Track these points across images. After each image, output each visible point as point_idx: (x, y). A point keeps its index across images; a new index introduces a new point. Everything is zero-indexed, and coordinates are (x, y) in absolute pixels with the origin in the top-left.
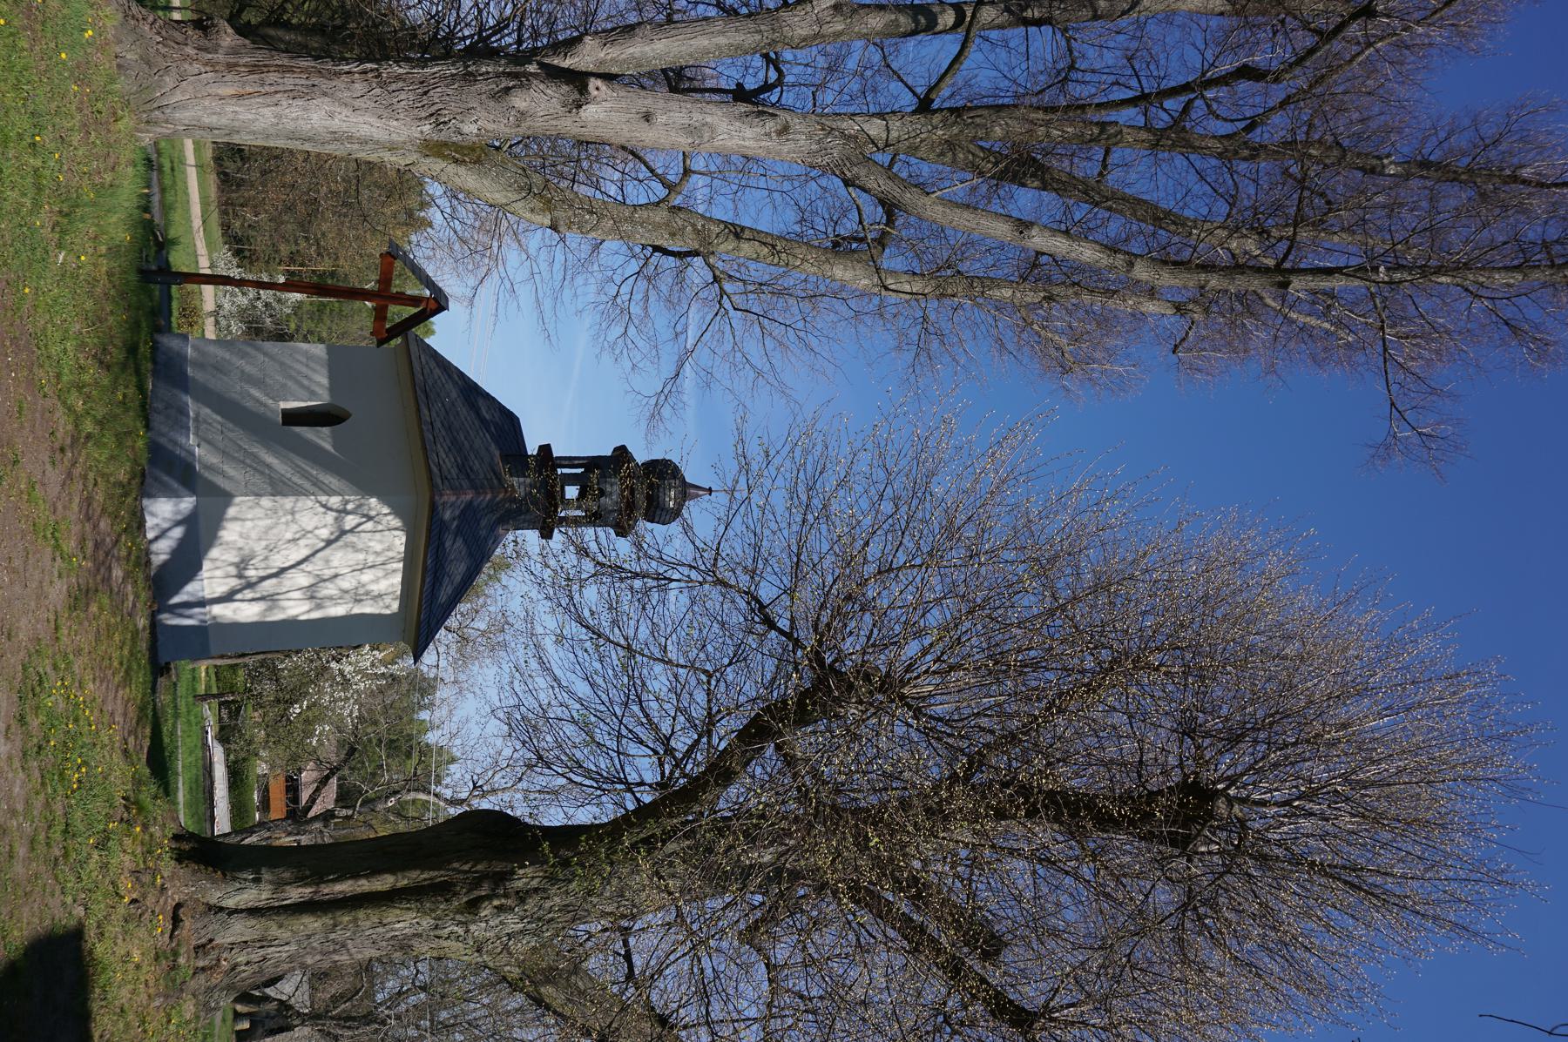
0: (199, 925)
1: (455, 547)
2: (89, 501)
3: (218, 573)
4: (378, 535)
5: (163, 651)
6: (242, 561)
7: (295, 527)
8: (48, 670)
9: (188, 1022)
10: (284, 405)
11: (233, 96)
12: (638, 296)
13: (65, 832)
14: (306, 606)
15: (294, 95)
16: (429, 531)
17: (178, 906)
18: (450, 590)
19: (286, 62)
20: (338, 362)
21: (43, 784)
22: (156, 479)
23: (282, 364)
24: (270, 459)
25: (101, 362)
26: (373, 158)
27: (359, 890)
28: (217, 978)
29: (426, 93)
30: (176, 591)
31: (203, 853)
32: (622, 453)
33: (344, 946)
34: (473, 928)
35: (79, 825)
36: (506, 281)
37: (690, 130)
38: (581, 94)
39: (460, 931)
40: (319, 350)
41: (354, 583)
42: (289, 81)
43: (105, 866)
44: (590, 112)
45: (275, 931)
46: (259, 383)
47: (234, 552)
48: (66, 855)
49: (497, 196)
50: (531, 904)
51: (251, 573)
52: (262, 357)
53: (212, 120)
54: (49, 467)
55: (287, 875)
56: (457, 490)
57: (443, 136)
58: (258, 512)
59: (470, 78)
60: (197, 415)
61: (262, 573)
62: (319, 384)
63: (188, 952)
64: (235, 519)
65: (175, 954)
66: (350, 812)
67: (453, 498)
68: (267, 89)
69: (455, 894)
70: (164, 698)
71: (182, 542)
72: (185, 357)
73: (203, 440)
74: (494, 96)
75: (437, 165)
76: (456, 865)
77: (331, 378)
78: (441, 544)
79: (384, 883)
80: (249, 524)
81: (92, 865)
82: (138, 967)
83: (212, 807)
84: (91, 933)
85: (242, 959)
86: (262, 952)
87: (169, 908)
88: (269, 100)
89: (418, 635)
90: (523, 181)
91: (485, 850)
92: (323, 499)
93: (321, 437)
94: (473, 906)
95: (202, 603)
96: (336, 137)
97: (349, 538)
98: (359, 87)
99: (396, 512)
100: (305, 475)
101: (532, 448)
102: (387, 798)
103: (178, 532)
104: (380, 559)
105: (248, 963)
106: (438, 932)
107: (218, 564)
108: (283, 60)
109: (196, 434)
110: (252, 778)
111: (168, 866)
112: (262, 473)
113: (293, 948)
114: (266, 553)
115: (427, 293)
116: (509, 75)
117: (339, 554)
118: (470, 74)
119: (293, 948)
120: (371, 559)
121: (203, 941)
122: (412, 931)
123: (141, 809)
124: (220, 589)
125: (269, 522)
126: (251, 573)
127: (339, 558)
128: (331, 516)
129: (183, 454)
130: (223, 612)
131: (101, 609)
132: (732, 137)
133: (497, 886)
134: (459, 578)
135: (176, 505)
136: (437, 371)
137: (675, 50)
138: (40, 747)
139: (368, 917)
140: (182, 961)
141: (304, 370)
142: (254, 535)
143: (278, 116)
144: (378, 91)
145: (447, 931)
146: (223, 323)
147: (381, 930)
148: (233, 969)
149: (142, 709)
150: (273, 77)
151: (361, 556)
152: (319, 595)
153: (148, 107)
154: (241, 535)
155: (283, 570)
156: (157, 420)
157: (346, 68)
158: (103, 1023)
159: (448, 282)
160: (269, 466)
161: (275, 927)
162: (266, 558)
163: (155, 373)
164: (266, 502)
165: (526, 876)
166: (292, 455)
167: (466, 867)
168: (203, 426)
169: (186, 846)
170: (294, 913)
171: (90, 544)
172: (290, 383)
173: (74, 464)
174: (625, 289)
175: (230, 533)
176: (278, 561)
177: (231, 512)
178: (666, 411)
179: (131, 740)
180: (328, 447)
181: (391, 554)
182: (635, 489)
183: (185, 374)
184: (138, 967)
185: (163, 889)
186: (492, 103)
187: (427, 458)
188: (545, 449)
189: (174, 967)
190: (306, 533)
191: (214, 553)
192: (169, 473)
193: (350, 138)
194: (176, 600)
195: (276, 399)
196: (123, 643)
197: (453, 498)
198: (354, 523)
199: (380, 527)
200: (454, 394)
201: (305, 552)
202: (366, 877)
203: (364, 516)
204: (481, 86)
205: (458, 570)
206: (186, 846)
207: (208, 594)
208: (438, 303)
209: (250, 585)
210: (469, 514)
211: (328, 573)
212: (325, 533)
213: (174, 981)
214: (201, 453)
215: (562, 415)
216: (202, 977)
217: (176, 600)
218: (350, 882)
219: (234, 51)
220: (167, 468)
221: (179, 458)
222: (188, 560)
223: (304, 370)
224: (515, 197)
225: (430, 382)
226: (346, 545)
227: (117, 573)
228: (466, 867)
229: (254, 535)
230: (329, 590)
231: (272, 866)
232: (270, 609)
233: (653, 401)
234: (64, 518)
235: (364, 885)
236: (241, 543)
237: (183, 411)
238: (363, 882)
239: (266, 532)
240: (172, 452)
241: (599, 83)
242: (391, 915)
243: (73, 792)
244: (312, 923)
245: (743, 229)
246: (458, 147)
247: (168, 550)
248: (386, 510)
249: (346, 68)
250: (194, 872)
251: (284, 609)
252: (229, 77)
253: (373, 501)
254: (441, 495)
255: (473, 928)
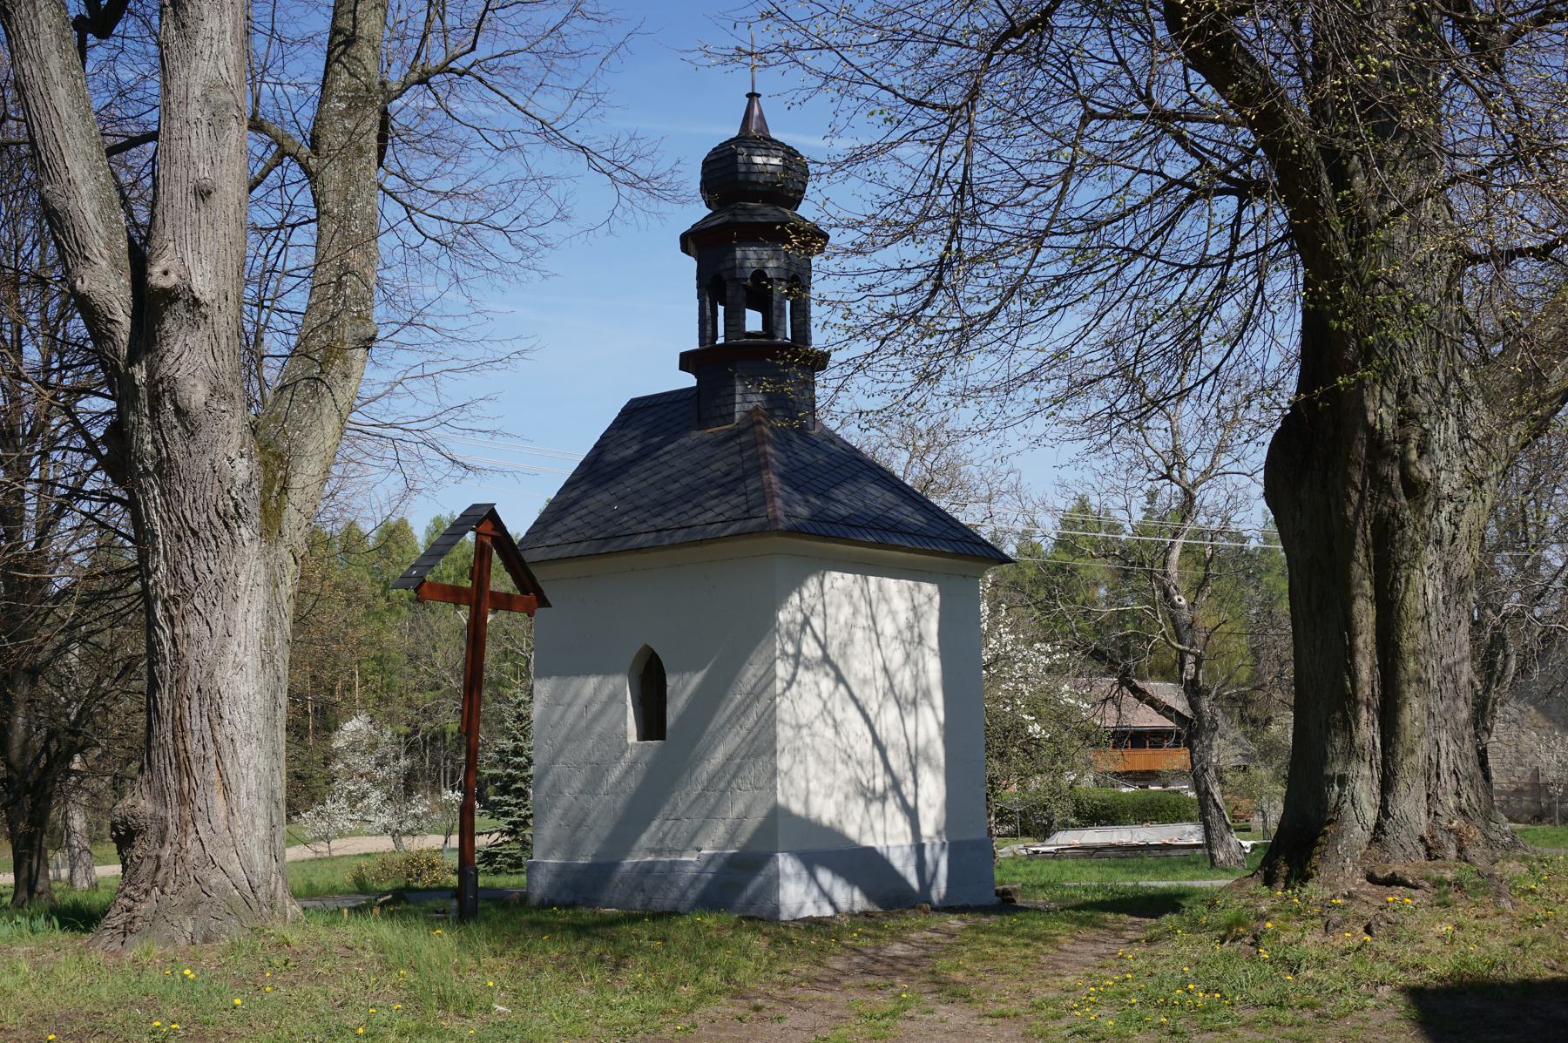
0: (1399, 854)
1: (845, 500)
2: (814, 982)
3: (878, 826)
4: (829, 611)
5: (982, 898)
6: (864, 795)
7: (818, 725)
8: (1064, 1023)
9: (1532, 870)
10: (632, 737)
11: (227, 798)
12: (445, 208)
13: (1280, 1006)
14: (925, 712)
15: (216, 717)
16: (827, 537)
17: (1371, 878)
18: (907, 510)
19: (167, 727)
20: (567, 662)
21: (1221, 1030)
22: (751, 903)
23: (567, 739)
24: (718, 757)
25: (617, 965)
26: (289, 608)
27: (1372, 647)
28: (1475, 833)
29: (195, 534)
30: (902, 880)
31: (1295, 849)
32: (692, 241)
33: (1449, 669)
34: (1446, 490)
35: (1270, 991)
36: (443, 418)
37: (217, 124)
38: (177, 299)
39: (1448, 508)
40: (543, 688)
41: (896, 644)
42: (195, 722)
43: (1321, 963)
44: (203, 286)
45: (1418, 760)
46: (598, 771)
47: (851, 805)
48: (1311, 1006)
49: (329, 429)
50: (1419, 403)
51: (880, 783)
52: (557, 768)
53: (261, 823)
54: (787, 1023)
55: (1338, 743)
56: (765, 497)
57: (255, 509)
58: (798, 772)
59: (165, 469)
60: (651, 851)
61: (880, 769)
62: (597, 690)
63: (1436, 868)
64: (806, 803)
65: (1438, 883)
66: (1190, 659)
67: (779, 502)
68: (211, 752)
69: (1394, 514)
70: (1041, 898)
71: (838, 871)
72: (563, 870)
73: (690, 842)
74: (191, 432)
75: (292, 519)
76: (1350, 512)
77: (587, 672)
78: (844, 521)
79: (1365, 614)
80: (813, 785)
81: (1322, 977)
82: (1459, 927)
83: (1147, 848)
84: (1415, 979)
85: (1451, 802)
86: (1445, 776)
87: (1375, 889)
88: (227, 749)
89: (974, 557)
90: (303, 390)
91: (1328, 461)
92: (779, 685)
93: (681, 689)
94: (1415, 489)
95: (919, 848)
96: (267, 661)
97: (833, 651)
98: (195, 627)
99: (797, 584)
100: (744, 709)
101: (689, 381)
102: (1173, 605)
103: (825, 877)
104: (864, 608)
105: (1458, 794)
106: (1446, 541)
107: (866, 826)
108: (165, 731)
109: (681, 853)
110: (1106, 793)
111: (1314, 890)
112: (740, 767)
113: (1444, 736)
114: (852, 764)
115: (470, 536)
116: (155, 410)
117: (856, 665)
118: (159, 467)
119: (1444, 736)
120: (862, 621)
121: (1421, 849)
122: (1439, 576)
123: (1238, 922)
124: (900, 824)
125: (811, 759)
126: (880, 783)
127: (862, 665)
128: (803, 675)
129: (712, 869)
130: (931, 819)
131: (958, 968)
132: (222, 53)
133: (1389, 453)
134: (889, 496)
135: (788, 877)
136: (569, 521)
137: (80, 143)
138: (1173, 1033)
139: (1415, 636)
140: (1449, 875)
141: (576, 709)
142: (828, 779)
143: (248, 738)
144: (198, 601)
145: (1446, 527)
146: (410, 824)
147: (1433, 619)
148: (1464, 813)
149: (1081, 923)
150: (193, 745)
151: (859, 635)
152: (911, 694)
153: (252, 900)
154: (828, 796)
155: (877, 742)
156: (661, 902)
157: (167, 645)
158: (1537, 966)
159: (454, 505)
160: (729, 759)
161: (1412, 759)
162: (860, 763)
163: (591, 903)
164: (783, 762)
165: (1381, 412)
166: (712, 727)
167: (1355, 497)
168: (668, 842)
169: (1284, 869)
170: (1397, 735)
171: (870, 980)
172: (598, 729)
173: (771, 997)
174: (433, 228)
175: (825, 810)
176: (864, 748)
177: (797, 807)
178: (643, 168)
179: (1130, 935)
180: (697, 679)
181: (856, 593)
182: (747, 219)
183: (588, 867)
184: (1459, 927)
185: (1350, 896)
186: (202, 436)
187: (716, 539)
188: (688, 361)
189: (1458, 885)
190: (826, 710)
191: (852, 831)
192: (742, 887)
193: (268, 641)
194: (913, 881)
195: (623, 748)
196: (996, 944)
197: (779, 502)
198: (813, 644)
199: (819, 608)
200: (605, 497)
201: (852, 711)
202: (1353, 637)
203: (803, 630)
204: (178, 450)
205: (877, 497)
206: (1284, 869)
207: (907, 840)
208: (485, 519)
209: (896, 785)
210: (798, 479)
211: (881, 681)
212: (827, 684)
213: (1477, 886)
214: (711, 845)
215: (648, 334)
216: (1471, 852)
217: (913, 881)
218: (1359, 659)
219: (161, 795)
220: (737, 886)
221: (717, 875)
222: (862, 865)
223: (576, 709)
224: (328, 400)
225: (589, 533)
226: (843, 655)
227: (898, 949)
228: (1355, 497)
229: (828, 779)
230: (904, 679)
231: (1323, 760)
232: (928, 759)
233: (625, 190)
234: (849, 1007)
235: (1365, 641)
236: (839, 796)
237: (647, 870)
238: (1360, 642)
239: (825, 763)
240: (710, 883)
241: (156, 271)
242: (1413, 602)
243: (1224, 997)
244: (1413, 711)
245: (335, 31)
246: (267, 489)
247: (848, 889)
248: (795, 599)
249: (167, 645)
250: (1324, 859)
251: (929, 741)
252: (200, 802)
253: (783, 616)
254: (776, 519)
255: (1446, 490)
